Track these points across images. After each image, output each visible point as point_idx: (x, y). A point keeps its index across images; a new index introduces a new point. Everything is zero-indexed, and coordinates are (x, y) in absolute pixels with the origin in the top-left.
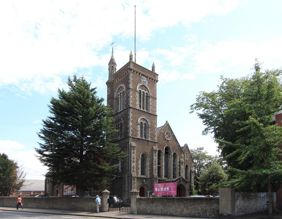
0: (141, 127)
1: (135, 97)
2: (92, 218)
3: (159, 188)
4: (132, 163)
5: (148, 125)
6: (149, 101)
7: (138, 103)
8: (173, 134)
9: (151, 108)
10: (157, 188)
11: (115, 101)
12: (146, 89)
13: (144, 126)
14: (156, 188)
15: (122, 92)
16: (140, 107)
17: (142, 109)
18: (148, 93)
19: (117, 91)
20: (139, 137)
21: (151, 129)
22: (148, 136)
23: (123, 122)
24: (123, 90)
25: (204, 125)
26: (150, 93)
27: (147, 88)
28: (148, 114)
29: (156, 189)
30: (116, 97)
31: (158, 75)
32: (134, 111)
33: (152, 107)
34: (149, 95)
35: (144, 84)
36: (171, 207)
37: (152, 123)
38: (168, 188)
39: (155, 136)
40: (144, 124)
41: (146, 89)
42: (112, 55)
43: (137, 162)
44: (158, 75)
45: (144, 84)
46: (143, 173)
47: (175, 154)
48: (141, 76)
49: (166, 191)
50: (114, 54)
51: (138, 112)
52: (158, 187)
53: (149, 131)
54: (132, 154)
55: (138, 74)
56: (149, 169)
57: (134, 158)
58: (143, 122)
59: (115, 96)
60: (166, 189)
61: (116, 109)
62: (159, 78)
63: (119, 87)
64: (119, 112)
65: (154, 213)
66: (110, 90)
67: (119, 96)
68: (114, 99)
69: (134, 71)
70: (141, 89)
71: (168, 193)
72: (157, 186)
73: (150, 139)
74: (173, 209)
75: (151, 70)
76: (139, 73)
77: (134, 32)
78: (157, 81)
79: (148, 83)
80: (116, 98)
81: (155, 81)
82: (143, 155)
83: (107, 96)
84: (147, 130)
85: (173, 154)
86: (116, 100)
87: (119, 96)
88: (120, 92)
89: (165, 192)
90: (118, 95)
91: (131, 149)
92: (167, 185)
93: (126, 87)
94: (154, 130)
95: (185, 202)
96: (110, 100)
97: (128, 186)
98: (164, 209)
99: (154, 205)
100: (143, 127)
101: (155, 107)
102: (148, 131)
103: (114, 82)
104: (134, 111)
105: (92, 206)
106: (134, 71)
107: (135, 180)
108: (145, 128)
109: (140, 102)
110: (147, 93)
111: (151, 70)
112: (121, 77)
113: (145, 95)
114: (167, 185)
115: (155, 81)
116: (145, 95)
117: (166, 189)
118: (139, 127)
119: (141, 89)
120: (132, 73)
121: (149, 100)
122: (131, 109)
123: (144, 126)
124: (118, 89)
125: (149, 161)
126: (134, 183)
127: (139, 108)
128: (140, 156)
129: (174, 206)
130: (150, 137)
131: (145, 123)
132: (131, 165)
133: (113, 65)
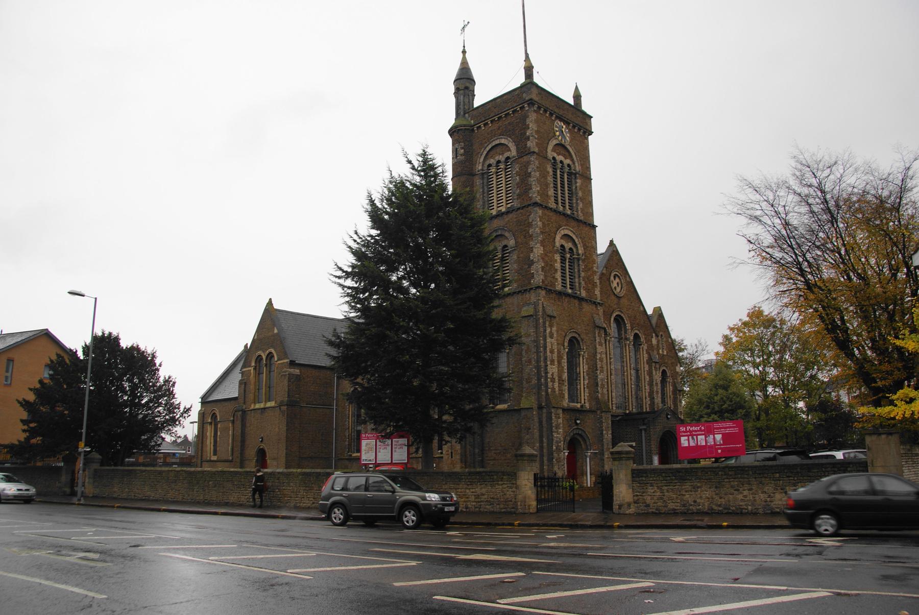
0: (563, 260)
1: (544, 175)
2: (860, 476)
3: (693, 439)
4: (549, 367)
5: (578, 255)
6: (576, 187)
7: (551, 192)
8: (628, 279)
9: (581, 205)
10: (686, 438)
11: (478, 181)
12: (568, 154)
13: (568, 256)
14: (683, 439)
15: (502, 158)
16: (556, 202)
17: (561, 208)
18: (571, 163)
19: (487, 154)
20: (559, 287)
21: (586, 266)
22: (580, 284)
23: (512, 243)
24: (507, 154)
25: (370, 196)
26: (577, 164)
27: (568, 151)
28: (574, 223)
29: (684, 441)
30: (482, 170)
31: (592, 117)
32: (545, 214)
33: (583, 203)
34: (575, 170)
35: (562, 140)
36: (738, 490)
37: (585, 247)
38: (719, 437)
39: (594, 285)
40: (567, 250)
41: (568, 154)
42: (464, 58)
43: (559, 362)
44: (592, 117)
45: (562, 140)
46: (573, 397)
47: (636, 336)
48: (555, 120)
49: (715, 444)
50: (467, 55)
51: (554, 217)
52: (691, 434)
53: (581, 269)
54: (549, 340)
55: (547, 115)
56: (586, 382)
57: (552, 352)
58: (566, 245)
59: (480, 168)
60: (714, 438)
61: (484, 202)
62: (595, 125)
63: (494, 144)
64: (494, 212)
65: (688, 510)
66: (462, 151)
67: (493, 170)
68: (474, 175)
69: (539, 108)
70: (555, 155)
71: (719, 451)
72: (686, 432)
73: (584, 294)
74: (745, 496)
75: (571, 101)
76: (550, 113)
77: (522, 7)
78: (591, 133)
79: (571, 140)
80: (483, 174)
81: (585, 133)
82: (571, 341)
83: (453, 165)
84: (576, 267)
85: (632, 338)
86: (483, 178)
87: (493, 170)
88: (497, 158)
89: (711, 447)
90: (490, 165)
91: (544, 323)
92: (717, 428)
93: (517, 145)
94: (592, 268)
95: (778, 475)
96: (456, 178)
97: (541, 436)
98: (717, 498)
99: (687, 486)
100: (565, 260)
101: (590, 204)
102: (579, 271)
103: (473, 130)
104: (545, 214)
105: (477, 497)
106: (539, 108)
107: (559, 418)
108: (571, 261)
109: (555, 188)
110: (569, 165)
111: (571, 101)
112: (500, 118)
113: (567, 169)
114: (717, 428)
115: (585, 133)
116: (567, 169)
117: (714, 438)
118: (558, 257)
119: (555, 155)
120: (535, 111)
121: (576, 183)
122: (537, 209)
123: (568, 256)
124: (488, 149)
125: (587, 359)
126: (557, 427)
127: (553, 206)
128: (566, 344)
129: (747, 486)
130: (585, 289)
131: (571, 249)
132: (546, 373)
133: (468, 85)
